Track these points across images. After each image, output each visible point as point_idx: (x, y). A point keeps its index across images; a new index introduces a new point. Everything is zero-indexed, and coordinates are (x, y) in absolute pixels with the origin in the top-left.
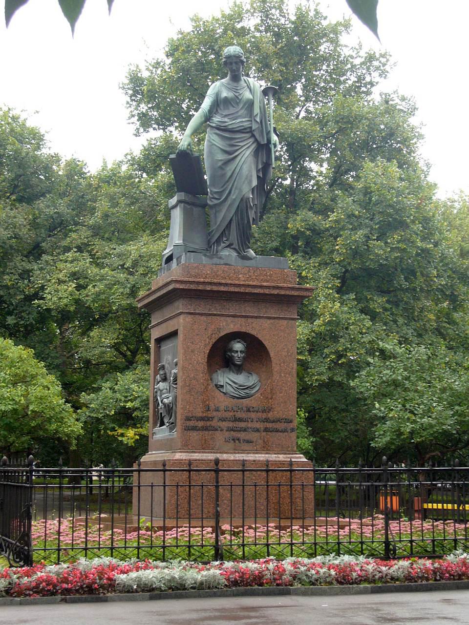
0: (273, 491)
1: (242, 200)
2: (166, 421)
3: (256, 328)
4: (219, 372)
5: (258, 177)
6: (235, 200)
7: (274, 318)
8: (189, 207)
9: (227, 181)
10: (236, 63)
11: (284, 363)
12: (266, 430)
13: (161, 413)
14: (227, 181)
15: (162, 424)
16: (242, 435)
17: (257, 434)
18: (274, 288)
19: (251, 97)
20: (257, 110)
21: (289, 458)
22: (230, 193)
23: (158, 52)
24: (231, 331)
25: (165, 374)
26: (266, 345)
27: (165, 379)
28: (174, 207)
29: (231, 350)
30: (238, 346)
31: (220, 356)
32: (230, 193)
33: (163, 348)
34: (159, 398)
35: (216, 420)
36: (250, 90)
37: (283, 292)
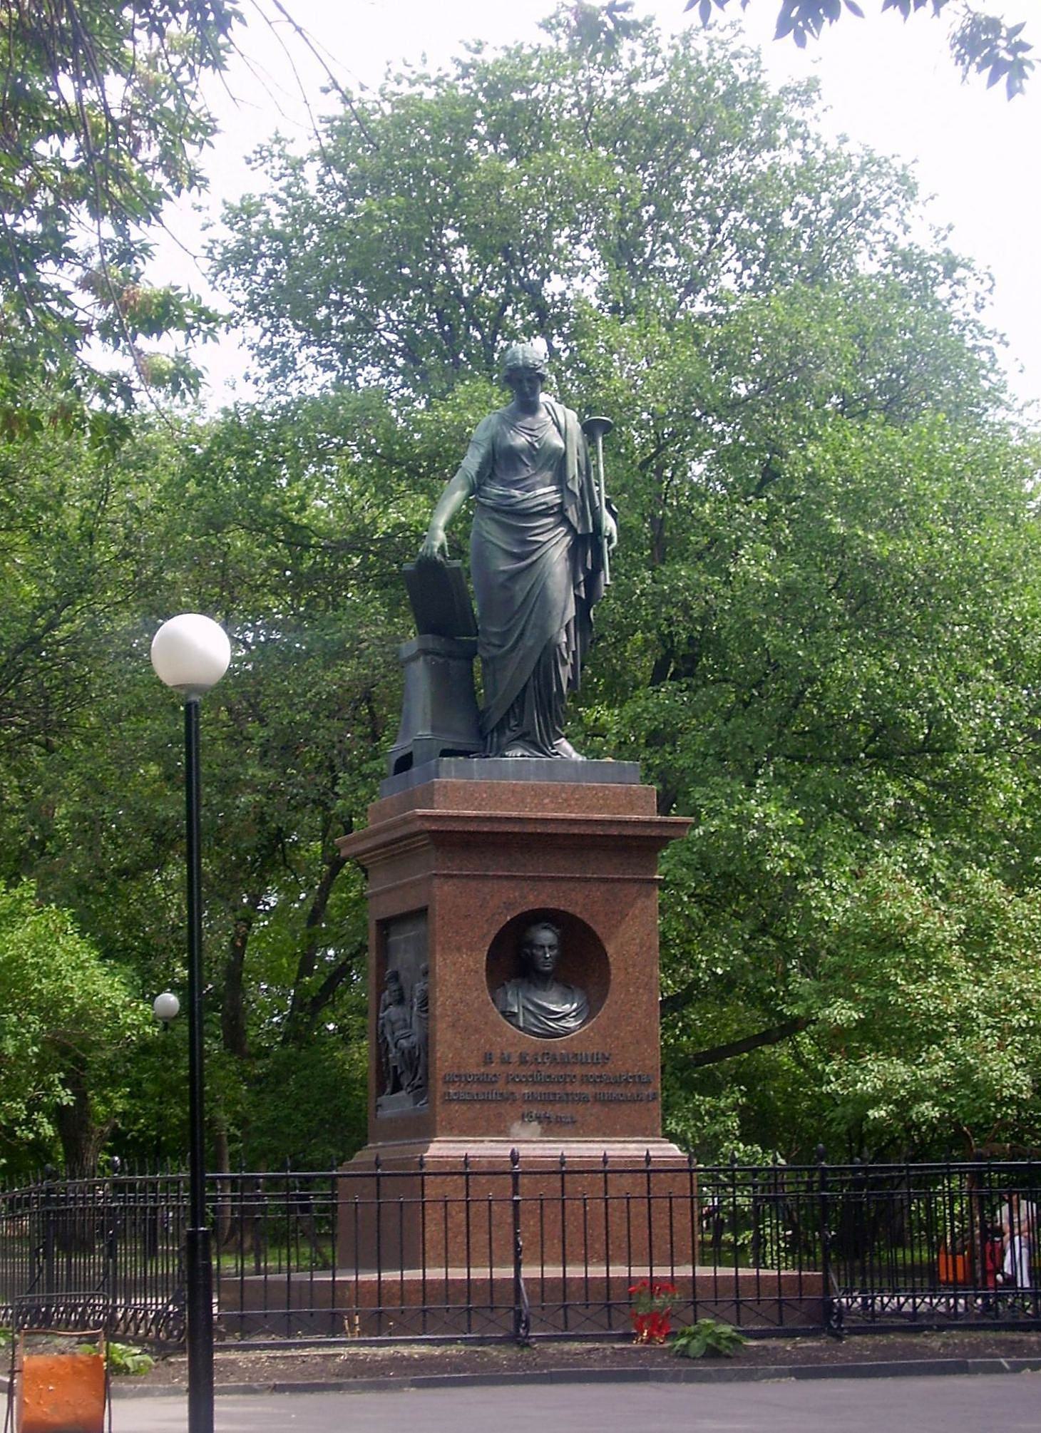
0: (574, 1206)
1: (545, 647)
2: (405, 1081)
3: (573, 901)
4: (508, 986)
5: (577, 598)
6: (532, 648)
7: (613, 880)
8: (441, 661)
9: (517, 612)
10: (529, 380)
11: (634, 966)
12: (598, 1099)
13: (395, 1067)
14: (517, 612)
15: (397, 1088)
16: (551, 1111)
17: (581, 1107)
18: (611, 822)
19: (562, 445)
20: (573, 469)
21: (642, 1149)
22: (522, 634)
23: (443, 63)
24: (570, 910)
25: (401, 989)
26: (599, 933)
27: (400, 1000)
28: (413, 658)
29: (531, 944)
30: (546, 936)
31: (512, 961)
32: (522, 634)
33: (392, 939)
34: (389, 1038)
35: (501, 1082)
36: (559, 431)
37: (629, 831)
